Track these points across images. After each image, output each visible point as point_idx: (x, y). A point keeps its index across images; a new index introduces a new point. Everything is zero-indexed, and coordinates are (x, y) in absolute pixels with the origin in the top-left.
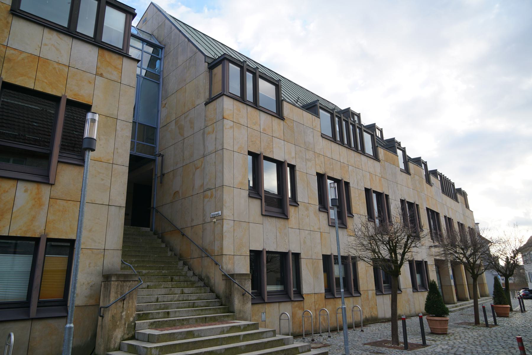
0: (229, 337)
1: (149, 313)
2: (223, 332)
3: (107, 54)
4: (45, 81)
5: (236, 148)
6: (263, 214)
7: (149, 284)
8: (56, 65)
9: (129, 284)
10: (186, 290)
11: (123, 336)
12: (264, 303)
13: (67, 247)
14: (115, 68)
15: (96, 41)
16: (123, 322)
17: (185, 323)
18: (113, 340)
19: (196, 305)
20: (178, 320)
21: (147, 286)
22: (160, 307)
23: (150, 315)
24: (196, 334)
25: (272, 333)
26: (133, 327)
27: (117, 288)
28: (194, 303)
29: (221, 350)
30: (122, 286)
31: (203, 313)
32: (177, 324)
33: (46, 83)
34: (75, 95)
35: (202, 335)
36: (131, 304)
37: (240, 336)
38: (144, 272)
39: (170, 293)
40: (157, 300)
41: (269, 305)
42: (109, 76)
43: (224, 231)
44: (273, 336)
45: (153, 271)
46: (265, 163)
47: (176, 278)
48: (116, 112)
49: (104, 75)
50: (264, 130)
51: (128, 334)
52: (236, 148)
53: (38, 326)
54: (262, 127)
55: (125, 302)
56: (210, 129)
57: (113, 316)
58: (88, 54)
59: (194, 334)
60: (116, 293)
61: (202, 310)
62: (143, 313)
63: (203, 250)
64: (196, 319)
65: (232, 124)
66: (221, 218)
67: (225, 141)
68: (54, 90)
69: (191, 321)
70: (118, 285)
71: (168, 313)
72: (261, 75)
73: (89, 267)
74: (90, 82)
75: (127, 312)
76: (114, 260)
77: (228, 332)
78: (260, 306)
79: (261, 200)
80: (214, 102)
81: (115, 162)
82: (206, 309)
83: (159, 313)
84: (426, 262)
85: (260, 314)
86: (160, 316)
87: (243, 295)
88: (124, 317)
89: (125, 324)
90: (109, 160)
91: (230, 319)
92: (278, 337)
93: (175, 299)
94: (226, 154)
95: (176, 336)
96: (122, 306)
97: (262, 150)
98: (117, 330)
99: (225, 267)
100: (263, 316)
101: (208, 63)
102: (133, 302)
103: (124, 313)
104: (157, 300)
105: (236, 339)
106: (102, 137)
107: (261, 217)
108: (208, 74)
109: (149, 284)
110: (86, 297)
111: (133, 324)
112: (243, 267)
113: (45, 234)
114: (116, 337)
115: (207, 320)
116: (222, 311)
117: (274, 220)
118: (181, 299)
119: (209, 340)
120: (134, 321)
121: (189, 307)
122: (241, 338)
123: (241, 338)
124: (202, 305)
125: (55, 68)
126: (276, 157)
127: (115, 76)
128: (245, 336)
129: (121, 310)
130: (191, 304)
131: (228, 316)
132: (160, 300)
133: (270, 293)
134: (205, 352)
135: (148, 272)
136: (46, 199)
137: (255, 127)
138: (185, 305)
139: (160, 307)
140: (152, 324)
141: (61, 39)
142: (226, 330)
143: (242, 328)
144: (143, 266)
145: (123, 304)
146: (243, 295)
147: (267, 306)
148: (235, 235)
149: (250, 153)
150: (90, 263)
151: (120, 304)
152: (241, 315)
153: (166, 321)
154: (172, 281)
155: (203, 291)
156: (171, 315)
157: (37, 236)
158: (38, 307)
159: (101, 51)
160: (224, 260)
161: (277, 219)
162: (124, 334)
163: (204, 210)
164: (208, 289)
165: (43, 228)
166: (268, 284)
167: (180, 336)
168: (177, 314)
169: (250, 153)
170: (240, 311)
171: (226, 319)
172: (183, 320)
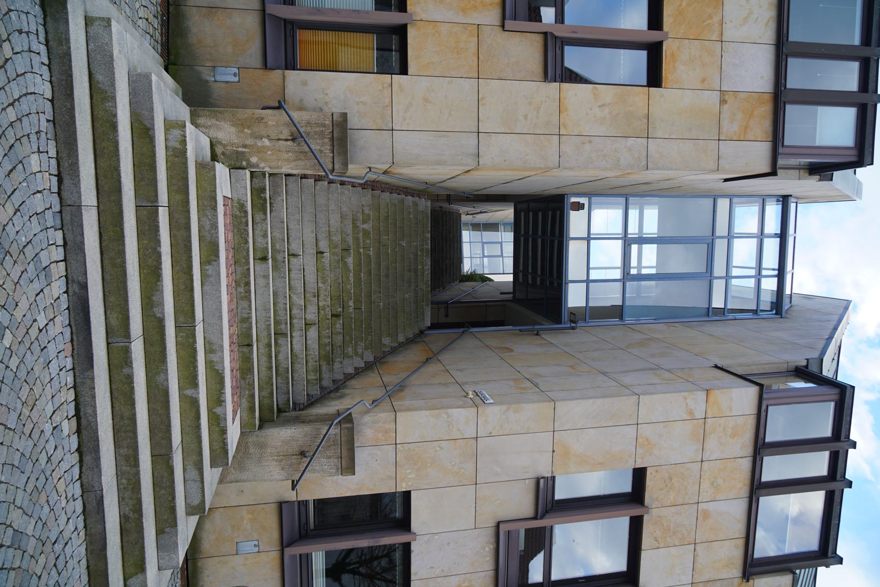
0: (195, 350)
1: (265, 214)
3: (766, 109)
4: (684, 4)
5: (646, 431)
6: (501, 526)
7: (327, 255)
8: (716, 19)
9: (327, 149)
10: (313, 333)
11: (220, 143)
12: (284, 544)
13: (392, 51)
14: (746, 127)
15: (781, 97)
16: (249, 142)
18: (214, 121)
19: (281, 341)
20: (249, 269)
21: (321, 250)
22: (279, 252)
23: (262, 216)
24: (210, 269)
25: (196, 502)
26: (238, 165)
27: (317, 125)
28: (286, 335)
29: (161, 304)
30: (321, 135)
31: (262, 350)
32: (239, 269)
33: (680, 5)
34: (673, 55)
36: (285, 156)
37: (196, 385)
38: (350, 261)
39: (308, 295)
40: (294, 255)
41: (277, 562)
42: (725, 116)
43: (450, 411)
44: (187, 505)
46: (621, 524)
47: (338, 326)
48: (659, 134)
49: (726, 107)
50: (706, 514)
51: (223, 154)
52: (646, 431)
53: (252, 22)
54: (711, 506)
55: (289, 143)
56: (667, 375)
57: (262, 118)
58: (754, 71)
59: (209, 263)
60: (308, 123)
62: (265, 200)
63: (401, 387)
64: (247, 320)
65: (700, 414)
66: (479, 401)
67: (655, 396)
68: (671, 20)
69: (245, 304)
70: (324, 126)
71: (264, 259)
72: (837, 494)
73: (358, 103)
74: (703, 81)
75: (268, 148)
76: (370, 156)
77: (209, 364)
78: (276, 535)
79: (535, 518)
81: (563, 138)
83: (265, 236)
84: (853, 388)
85: (255, 536)
86: (259, 239)
87: (303, 454)
88: (259, 144)
89: (245, 146)
90: (565, 127)
91: (245, 415)
92: (186, 527)
93: (294, 297)
94: (625, 403)
95: (209, 213)
96: (282, 137)
97: (655, 512)
98: (233, 130)
99: (367, 418)
100: (248, 547)
101: (807, 367)
102: (288, 161)
103: (266, 142)
104: (294, 255)
105: (189, 378)
106: (606, 110)
107: (492, 523)
108: (784, 367)
110: (301, 100)
111: (244, 163)
112: (368, 478)
114: (219, 129)
115: (246, 349)
116: (266, 401)
117: (487, 564)
118: (294, 312)
119: (192, 290)
120: (250, 165)
121: (276, 323)
122: (189, 392)
123: (189, 392)
124: (281, 357)
125: (710, 17)
126: (646, 557)
127: (730, 127)
128: (194, 403)
129: (273, 136)
130: (283, 327)
131: (252, 409)
132: (294, 260)
133: (306, 561)
134: (159, 255)
135: (348, 270)
136: (476, 18)
137: (705, 485)
138: (281, 313)
139: (279, 252)
140: (242, 207)
141: (767, 24)
142: (214, 358)
143: (218, 410)
144: (360, 265)
145: (286, 140)
146: (303, 454)
147: (274, 556)
148: (444, 444)
149: (639, 475)
150: (365, 104)
151: (286, 134)
152: (252, 450)
153: (247, 242)
154: (332, 315)
155: (312, 377)
156: (261, 267)
157: (409, 8)
158: (285, 20)
159: (768, 98)
160: (383, 415)
161: (491, 573)
162: (225, 146)
163: (488, 381)
164: (316, 391)
165: (424, 16)
166: (328, 554)
168: (261, 282)
169: (639, 475)
170: (262, 446)
171: (245, 403)
172: (248, 284)
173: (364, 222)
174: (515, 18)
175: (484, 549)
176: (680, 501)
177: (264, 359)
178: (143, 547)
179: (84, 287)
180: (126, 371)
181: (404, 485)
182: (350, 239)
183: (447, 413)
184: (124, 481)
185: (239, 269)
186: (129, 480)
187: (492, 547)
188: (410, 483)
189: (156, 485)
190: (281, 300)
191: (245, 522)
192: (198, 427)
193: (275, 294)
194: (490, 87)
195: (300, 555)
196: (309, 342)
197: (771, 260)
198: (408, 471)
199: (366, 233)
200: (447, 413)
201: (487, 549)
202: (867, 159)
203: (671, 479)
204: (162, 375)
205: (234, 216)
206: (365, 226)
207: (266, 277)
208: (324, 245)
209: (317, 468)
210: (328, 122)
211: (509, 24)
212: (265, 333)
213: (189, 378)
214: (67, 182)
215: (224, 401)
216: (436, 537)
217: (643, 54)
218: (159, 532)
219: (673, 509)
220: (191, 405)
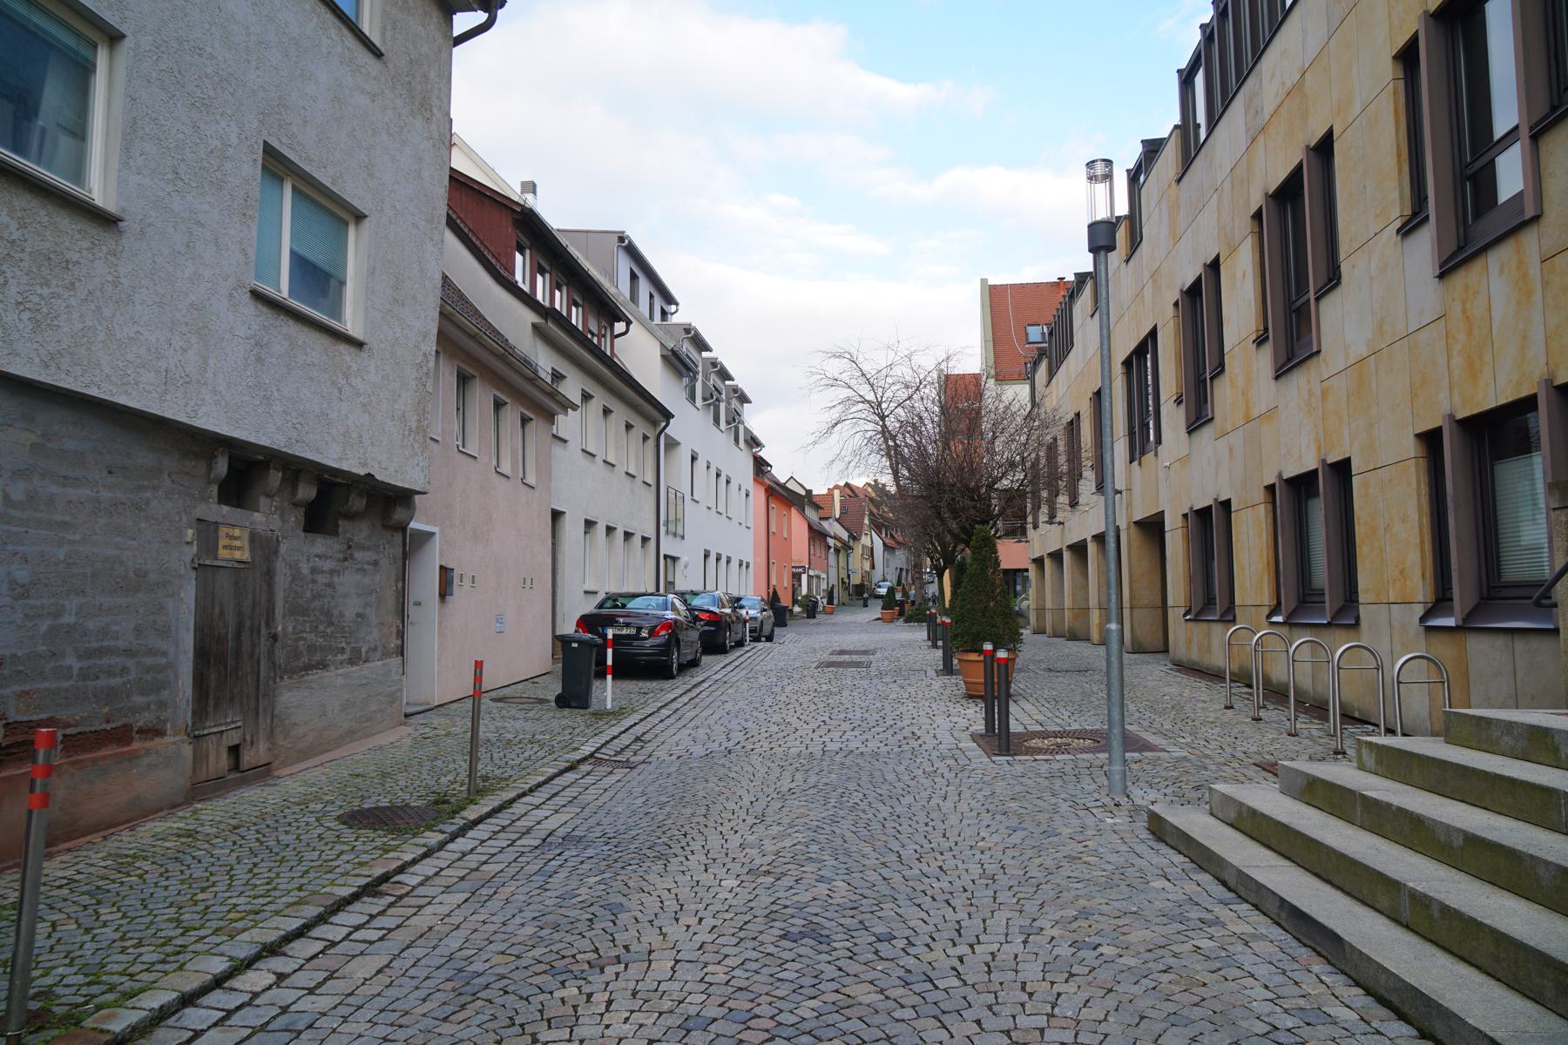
167: (1507, 740)
204: (1541, 870)
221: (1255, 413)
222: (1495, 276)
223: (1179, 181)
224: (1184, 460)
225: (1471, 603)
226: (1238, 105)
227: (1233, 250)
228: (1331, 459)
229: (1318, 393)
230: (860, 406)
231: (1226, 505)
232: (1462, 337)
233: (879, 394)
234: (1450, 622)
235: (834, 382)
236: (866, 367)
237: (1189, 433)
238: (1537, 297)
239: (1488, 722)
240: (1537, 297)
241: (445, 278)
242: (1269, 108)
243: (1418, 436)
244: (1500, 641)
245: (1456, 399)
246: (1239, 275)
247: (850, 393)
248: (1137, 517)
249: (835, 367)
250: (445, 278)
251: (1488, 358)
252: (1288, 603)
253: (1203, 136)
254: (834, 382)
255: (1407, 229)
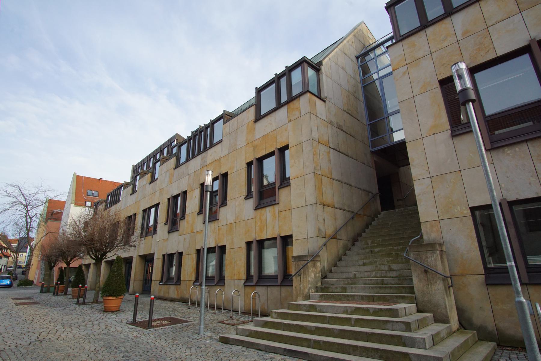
0: (337, 317)
2: (346, 312)
7: (364, 261)
8: (271, 133)
10: (394, 267)
17: (350, 299)
24: (318, 309)
25: (404, 326)
29: (311, 326)
30: (298, 265)
35: (324, 310)
37: (350, 319)
45: (384, 249)
49: (292, 119)
59: (316, 309)
60: (295, 270)
61: (380, 288)
64: (362, 296)
69: (356, 297)
71: (345, 288)
77: (352, 313)
80: (295, 102)
82: (385, 287)
83: (337, 288)
86: (338, 290)
87: (426, 272)
93: (372, 275)
103: (301, 286)
109: (364, 261)
113: (279, 235)
121: (377, 284)
122: (353, 322)
124: (393, 282)
128: (357, 320)
132: (357, 275)
142: (349, 311)
143: (371, 311)
148: (436, 194)
167: (305, 308)
168: (354, 290)
172: (348, 296)
173: (368, 244)
174: (275, 200)
175: (509, 154)
176: (458, 52)
177: (387, 290)
178: (395, 352)
179: (285, 349)
180: (321, 343)
181: (465, 212)
182: (367, 250)
183: (418, 196)
184: (364, 354)
185: (343, 299)
186: (363, 352)
187: (507, 149)
188: (464, 208)
189: (380, 342)
190: (367, 282)
191: (504, 307)
192: (367, 320)
193: (365, 284)
194: (294, 205)
195: (528, 272)
196: (399, 268)
197: (389, 43)
198: (456, 211)
199: (372, 243)
200: (418, 196)
201: (509, 152)
202: (303, 59)
203: (444, 64)
204: (335, 331)
205: (325, 299)
206: (369, 243)
207: (352, 288)
208: (361, 263)
209: (433, 263)
210: (294, 263)
211: (277, 202)
212: (375, 289)
213: (347, 321)
214: (260, 348)
215: (367, 308)
216: (503, 186)
217: (477, 75)
218: (404, 345)
219: (464, 54)
220: (358, 322)
221: (195, 231)
222: (268, 213)
223: (174, 169)
224: (166, 240)
225: (257, 280)
226: (199, 158)
227: (192, 190)
228: (220, 245)
229: (217, 229)
230: (19, 205)
231: (180, 254)
232: (259, 223)
233: (28, 203)
234: (198, 284)
235: (9, 195)
236: (25, 192)
237: (169, 233)
238: (277, 218)
239: (300, 305)
240: (277, 218)
241: (150, 183)
242: (209, 162)
243: (246, 242)
244: (264, 288)
245: (257, 236)
246: (194, 196)
247: (15, 200)
248: (140, 254)
249: (10, 189)
250: (150, 183)
251: (265, 228)
252: (164, 280)
253: (183, 159)
254: (9, 195)
255: (247, 198)
